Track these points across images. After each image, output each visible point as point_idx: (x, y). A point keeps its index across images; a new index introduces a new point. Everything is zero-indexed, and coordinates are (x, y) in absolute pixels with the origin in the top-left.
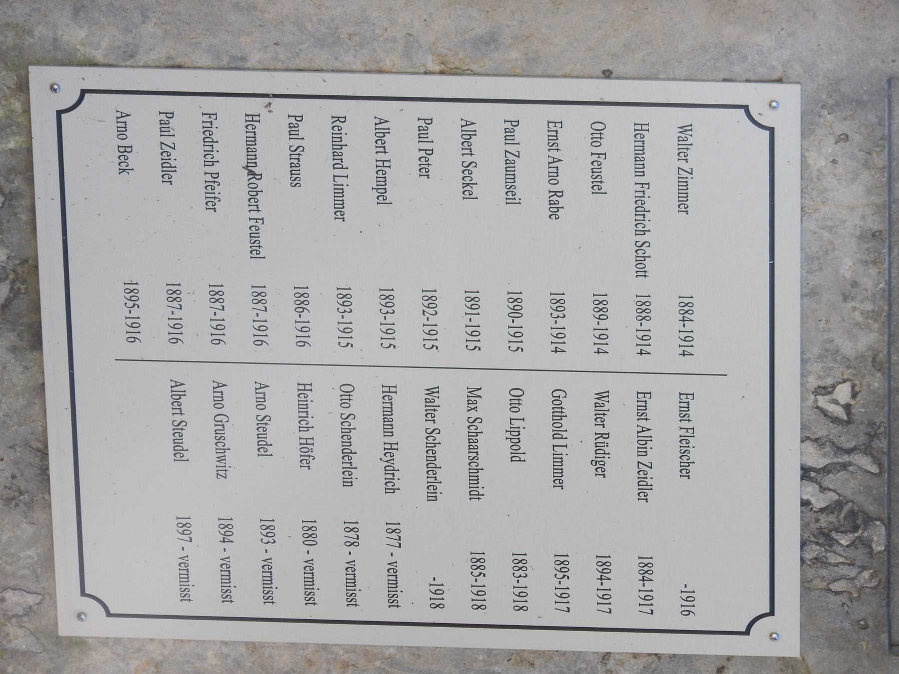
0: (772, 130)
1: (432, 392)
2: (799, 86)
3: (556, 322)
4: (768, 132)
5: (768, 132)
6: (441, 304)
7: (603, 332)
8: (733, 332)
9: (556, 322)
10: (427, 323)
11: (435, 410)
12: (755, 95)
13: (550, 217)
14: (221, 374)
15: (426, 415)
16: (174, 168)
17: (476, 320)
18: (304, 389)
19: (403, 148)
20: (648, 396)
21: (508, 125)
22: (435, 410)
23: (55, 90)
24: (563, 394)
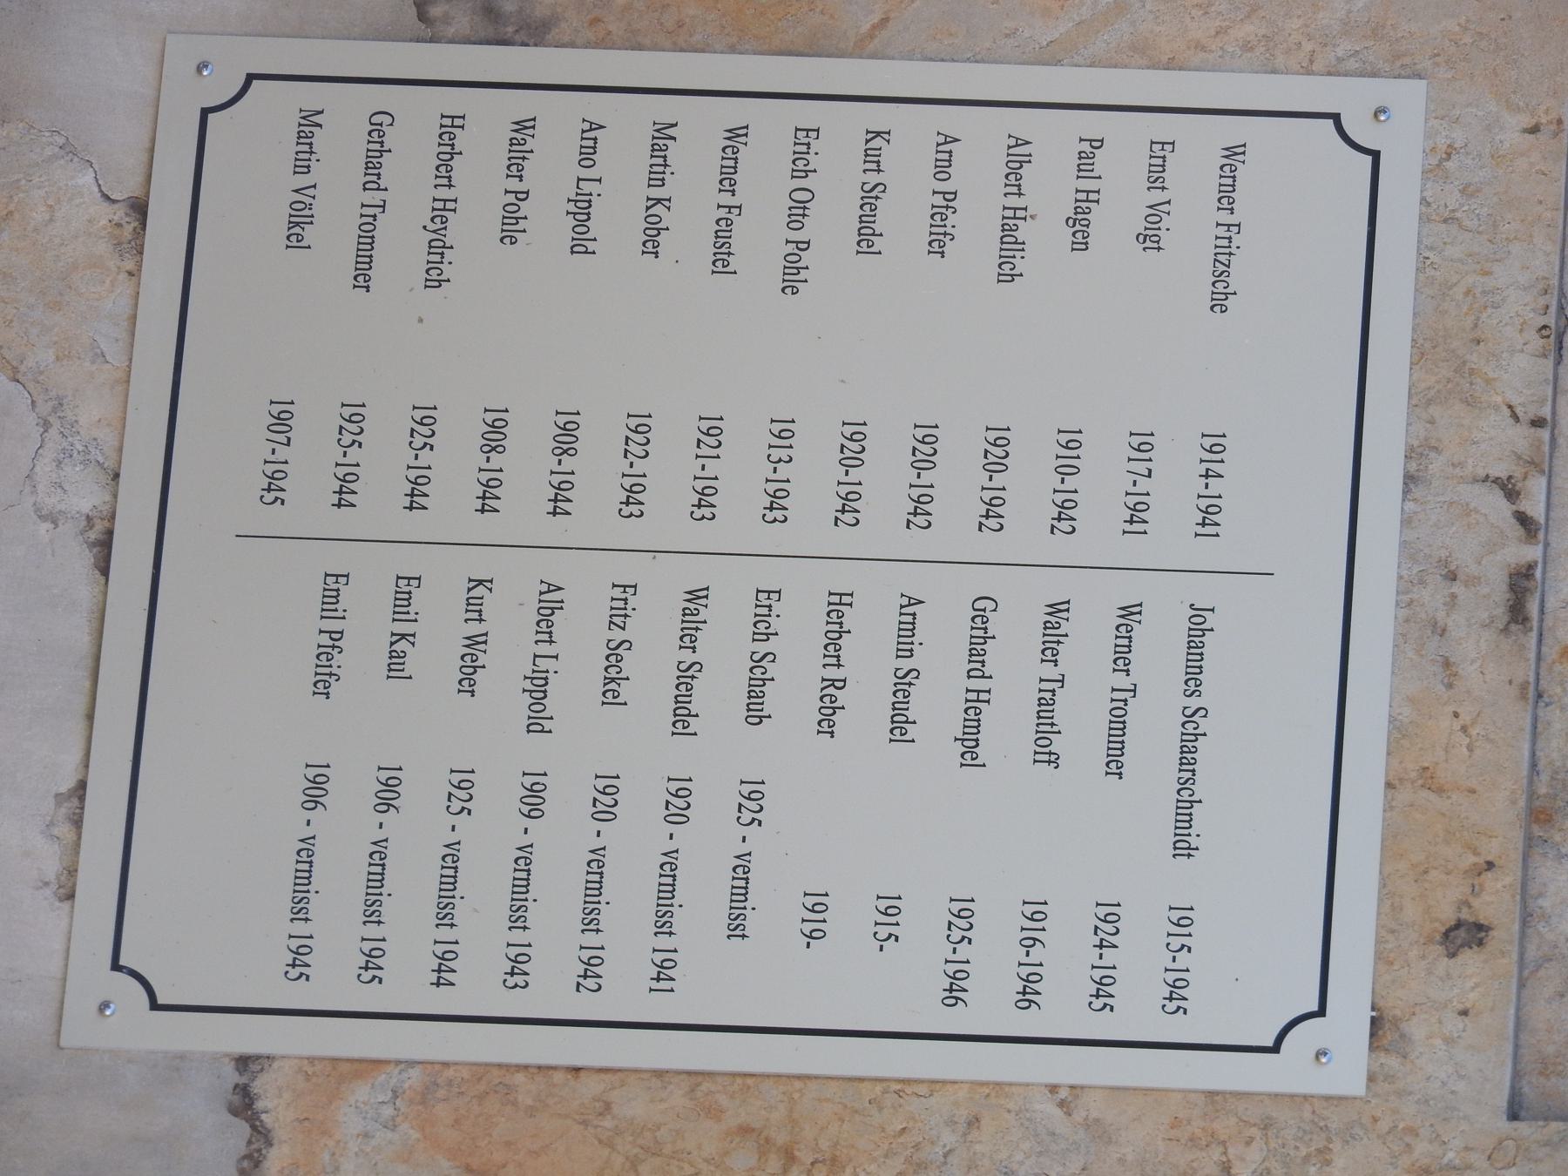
0: (1376, 155)
1: (1129, 612)
2: (1422, 85)
3: (775, 470)
4: (1370, 158)
5: (1370, 158)
6: (300, 426)
7: (997, 493)
8: (1287, 505)
9: (775, 470)
10: (1133, 490)
11: (1059, 642)
12: (1352, 97)
13: (1212, 308)
14: (554, 567)
15: (1043, 652)
16: (1071, 221)
17: (712, 467)
18: (839, 603)
19: (1048, 189)
20: (774, 596)
21: (1086, 146)
22: (1059, 642)
23: (199, 70)
24: (991, 605)
